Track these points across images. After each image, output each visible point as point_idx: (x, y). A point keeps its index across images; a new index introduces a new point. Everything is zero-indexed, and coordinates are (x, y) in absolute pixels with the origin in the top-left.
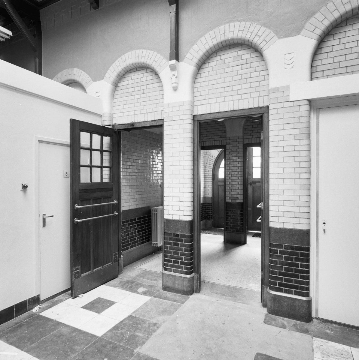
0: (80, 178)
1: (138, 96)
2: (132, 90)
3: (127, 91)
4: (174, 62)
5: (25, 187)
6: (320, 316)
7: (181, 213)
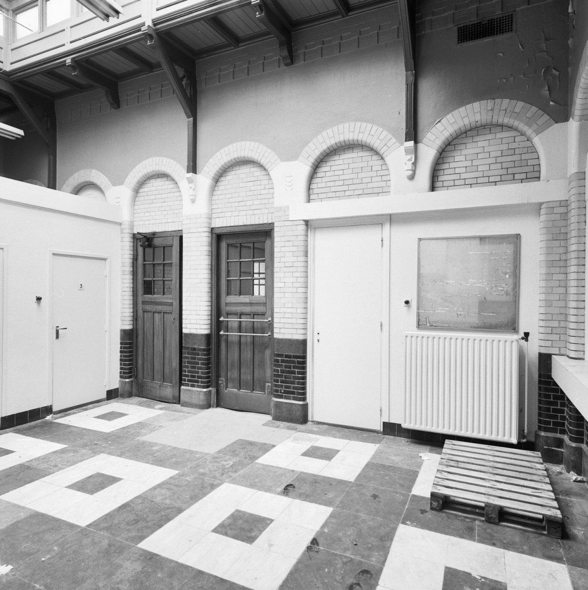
0: (456, 209)
1: (159, 205)
2: (154, 197)
3: (147, 198)
4: (191, 175)
5: (39, 299)
6: (316, 419)
7: (198, 326)
